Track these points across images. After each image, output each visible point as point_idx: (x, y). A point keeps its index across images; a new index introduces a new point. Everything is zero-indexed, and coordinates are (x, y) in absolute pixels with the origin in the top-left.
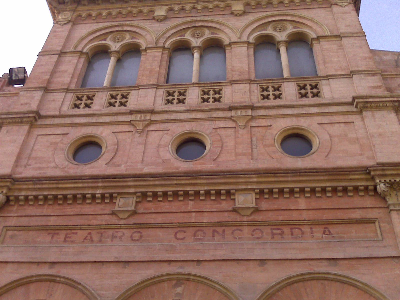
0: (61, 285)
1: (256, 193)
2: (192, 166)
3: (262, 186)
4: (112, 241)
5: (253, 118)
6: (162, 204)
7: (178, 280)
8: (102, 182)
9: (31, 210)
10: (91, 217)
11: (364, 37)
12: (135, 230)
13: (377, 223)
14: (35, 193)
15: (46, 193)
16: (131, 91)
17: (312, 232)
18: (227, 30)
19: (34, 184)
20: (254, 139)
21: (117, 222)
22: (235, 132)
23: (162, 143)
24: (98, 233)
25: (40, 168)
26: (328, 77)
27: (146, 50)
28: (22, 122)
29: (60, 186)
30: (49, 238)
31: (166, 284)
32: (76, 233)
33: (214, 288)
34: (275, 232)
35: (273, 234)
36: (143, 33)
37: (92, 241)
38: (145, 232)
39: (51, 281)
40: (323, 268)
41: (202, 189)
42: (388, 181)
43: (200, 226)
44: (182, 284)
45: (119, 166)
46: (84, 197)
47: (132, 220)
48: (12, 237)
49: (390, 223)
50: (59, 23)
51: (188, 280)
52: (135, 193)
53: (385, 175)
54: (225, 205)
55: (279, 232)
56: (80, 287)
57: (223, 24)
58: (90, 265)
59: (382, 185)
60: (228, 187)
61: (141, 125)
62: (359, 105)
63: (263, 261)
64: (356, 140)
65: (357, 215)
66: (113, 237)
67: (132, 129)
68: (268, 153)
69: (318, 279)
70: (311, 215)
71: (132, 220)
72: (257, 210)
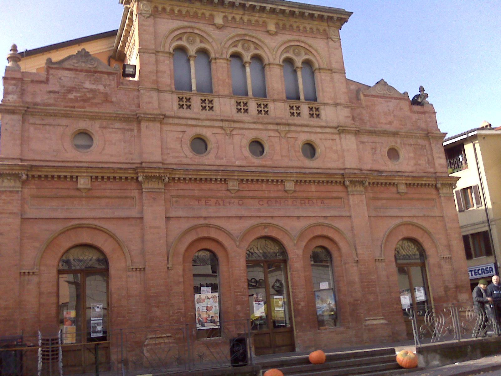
0: (212, 228)
1: (294, 182)
2: (261, 162)
3: (297, 179)
4: (230, 205)
5: (289, 131)
6: (250, 185)
7: (265, 226)
8: (221, 173)
9: (182, 186)
10: (216, 191)
11: (344, 74)
12: (239, 199)
13: (342, 199)
14: (184, 177)
15: (190, 177)
16: (214, 98)
17: (317, 203)
18: (265, 49)
19: (184, 172)
20: (290, 146)
21: (230, 195)
22: (279, 140)
23: (243, 144)
24: (221, 200)
25: (177, 157)
26: (325, 104)
27: (215, 59)
28: (155, 121)
29: (199, 173)
30: (197, 203)
31: (260, 228)
32: (210, 200)
33: (280, 229)
34: (302, 202)
35: (301, 203)
36: (210, 40)
37: (219, 205)
38: (246, 201)
39: (207, 227)
40: (321, 221)
41: (270, 179)
42: (350, 180)
43: (269, 199)
44: (267, 227)
45: (222, 159)
46: (211, 179)
47: (238, 194)
48: (176, 202)
49: (348, 200)
50: (143, 15)
51: (269, 226)
52: (238, 179)
53: (350, 177)
54: (280, 187)
55: (304, 202)
56: (223, 229)
57: (263, 42)
58: (224, 218)
59: (348, 182)
60: (282, 179)
61: (229, 130)
62: (340, 131)
63: (298, 217)
64: (336, 152)
65: (335, 195)
66: (230, 203)
67: (223, 132)
68: (297, 157)
69: (320, 225)
70: (317, 194)
71: (238, 194)
72: (295, 191)
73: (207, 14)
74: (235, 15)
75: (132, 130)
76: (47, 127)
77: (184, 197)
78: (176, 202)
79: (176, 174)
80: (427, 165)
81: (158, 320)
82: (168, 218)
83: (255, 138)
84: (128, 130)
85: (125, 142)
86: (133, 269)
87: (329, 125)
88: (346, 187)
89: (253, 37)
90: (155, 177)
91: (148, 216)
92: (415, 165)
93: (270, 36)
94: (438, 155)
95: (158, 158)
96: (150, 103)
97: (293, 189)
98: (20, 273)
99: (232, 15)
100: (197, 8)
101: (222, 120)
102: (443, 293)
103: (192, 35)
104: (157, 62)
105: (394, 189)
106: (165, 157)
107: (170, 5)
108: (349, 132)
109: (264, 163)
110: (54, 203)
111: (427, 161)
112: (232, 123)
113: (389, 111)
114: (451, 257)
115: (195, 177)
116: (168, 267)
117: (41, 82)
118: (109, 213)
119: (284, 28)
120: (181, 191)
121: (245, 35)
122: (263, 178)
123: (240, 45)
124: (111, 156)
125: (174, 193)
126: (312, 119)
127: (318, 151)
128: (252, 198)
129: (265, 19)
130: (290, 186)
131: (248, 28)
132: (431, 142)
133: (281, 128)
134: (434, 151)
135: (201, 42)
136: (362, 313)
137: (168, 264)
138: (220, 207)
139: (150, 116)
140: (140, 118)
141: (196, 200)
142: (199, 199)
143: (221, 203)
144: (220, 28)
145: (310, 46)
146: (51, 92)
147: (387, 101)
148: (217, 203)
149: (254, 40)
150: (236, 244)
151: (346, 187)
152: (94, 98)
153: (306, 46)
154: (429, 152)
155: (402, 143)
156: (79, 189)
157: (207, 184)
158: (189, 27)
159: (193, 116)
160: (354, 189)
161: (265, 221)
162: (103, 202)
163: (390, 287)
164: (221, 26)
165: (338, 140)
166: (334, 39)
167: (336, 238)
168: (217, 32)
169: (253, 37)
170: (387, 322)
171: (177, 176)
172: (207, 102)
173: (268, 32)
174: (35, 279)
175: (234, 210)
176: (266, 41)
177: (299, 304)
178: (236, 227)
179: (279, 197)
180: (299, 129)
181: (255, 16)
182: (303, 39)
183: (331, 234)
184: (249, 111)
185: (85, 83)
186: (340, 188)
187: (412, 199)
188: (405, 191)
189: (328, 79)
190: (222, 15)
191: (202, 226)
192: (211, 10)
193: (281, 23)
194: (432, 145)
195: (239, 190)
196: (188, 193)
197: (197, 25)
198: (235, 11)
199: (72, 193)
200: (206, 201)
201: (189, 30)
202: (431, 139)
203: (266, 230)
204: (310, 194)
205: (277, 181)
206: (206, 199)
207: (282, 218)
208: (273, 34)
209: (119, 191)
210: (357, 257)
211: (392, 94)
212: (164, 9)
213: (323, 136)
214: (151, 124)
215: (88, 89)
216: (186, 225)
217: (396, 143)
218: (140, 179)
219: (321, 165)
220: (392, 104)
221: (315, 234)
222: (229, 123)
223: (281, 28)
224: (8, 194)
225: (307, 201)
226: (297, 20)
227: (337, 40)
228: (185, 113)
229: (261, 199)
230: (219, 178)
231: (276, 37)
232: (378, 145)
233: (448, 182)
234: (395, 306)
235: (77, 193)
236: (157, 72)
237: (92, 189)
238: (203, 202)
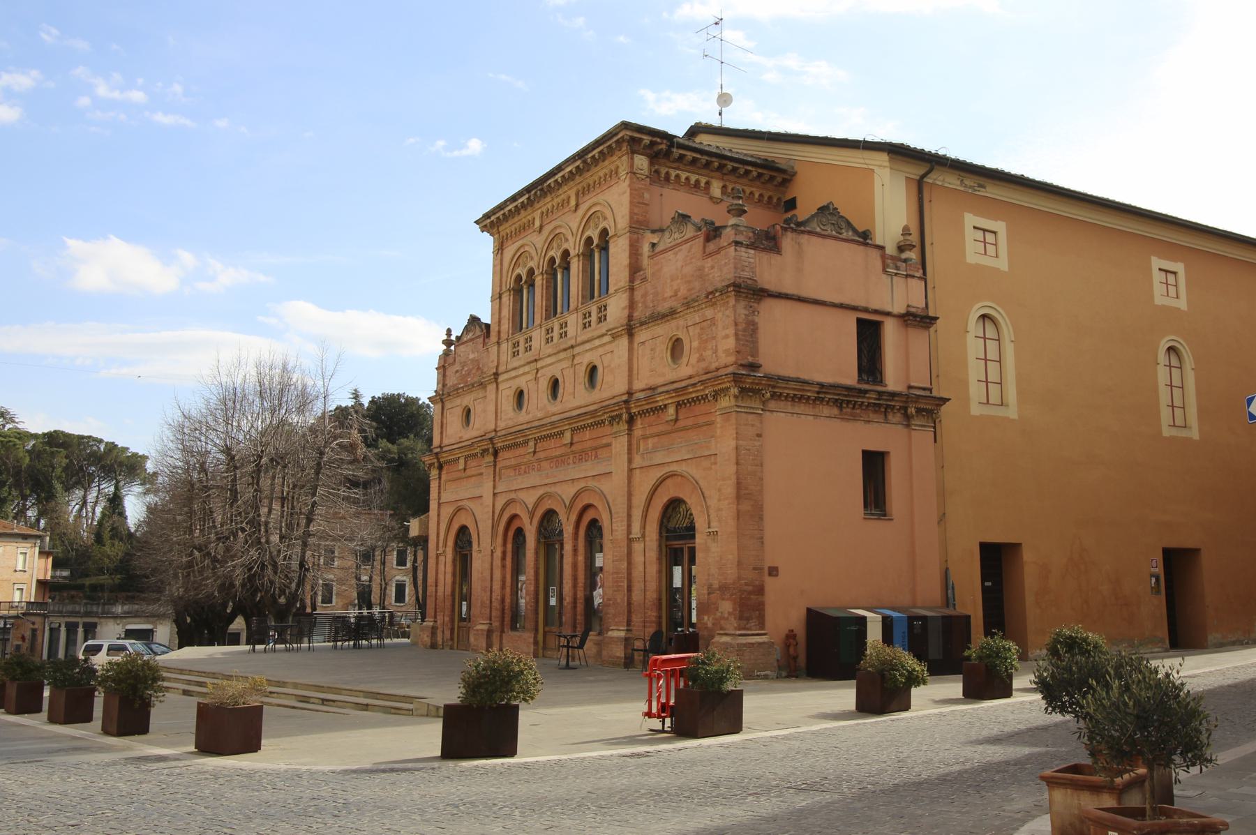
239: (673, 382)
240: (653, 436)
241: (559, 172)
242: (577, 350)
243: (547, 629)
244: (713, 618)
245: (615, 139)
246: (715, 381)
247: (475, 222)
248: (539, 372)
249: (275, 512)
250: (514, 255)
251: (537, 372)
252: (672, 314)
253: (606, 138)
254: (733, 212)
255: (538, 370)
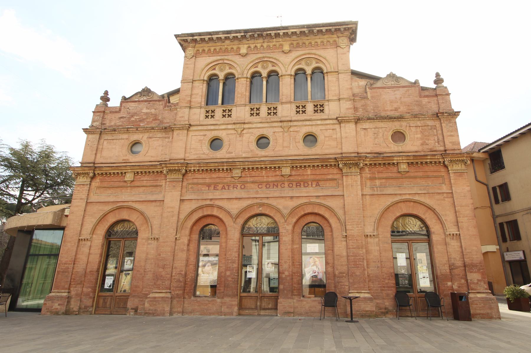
18: (280, 65)
21: (234, 181)
27: (238, 79)
30: (207, 188)
32: (218, 186)
36: (235, 66)
40: (313, 200)
43: (268, 183)
45: (232, 153)
48: (192, 188)
57: (278, 60)
60: (279, 165)
63: (292, 197)
65: (330, 177)
70: (312, 177)
72: (290, 175)
73: (235, 47)
74: (256, 44)
75: (169, 138)
76: (115, 141)
77: (198, 184)
78: (192, 188)
79: (191, 167)
80: (437, 144)
81: (162, 278)
82: (182, 201)
83: (305, 134)
84: (166, 138)
85: (162, 146)
86: (151, 238)
87: (330, 117)
88: (341, 170)
89: (270, 58)
90: (175, 170)
91: (168, 200)
92: (422, 144)
93: (285, 54)
94: (449, 134)
95: (182, 156)
96: (182, 117)
97: (289, 174)
98: (79, 239)
99: (254, 45)
100: (227, 45)
101: (234, 124)
102: (448, 271)
103: (222, 64)
104: (192, 88)
105: (395, 169)
106: (187, 155)
107: (208, 47)
108: (348, 121)
109: (267, 154)
110: (109, 191)
111: (436, 140)
112: (290, 122)
113: (396, 98)
114: (459, 234)
115: (206, 168)
116: (176, 238)
117: (116, 112)
118: (143, 198)
119: (298, 46)
120: (196, 180)
121: (264, 57)
122: (262, 166)
123: (260, 66)
124: (152, 157)
125: (191, 181)
126: (316, 114)
127: (319, 140)
128: (253, 182)
129: (281, 42)
130: (286, 171)
131: (268, 52)
132: (442, 122)
133: (285, 124)
134: (445, 130)
135: (230, 68)
136: (346, 286)
137: (176, 235)
138: (225, 191)
139: (179, 126)
140: (172, 129)
141: (207, 186)
142: (209, 185)
143: (227, 188)
144: (244, 56)
145: (320, 56)
146: (121, 118)
147: (395, 91)
148: (224, 188)
149: (271, 60)
150: (233, 220)
151: (446, 166)
152: (147, 118)
153: (316, 57)
154: (440, 132)
155: (408, 125)
156: (125, 182)
157: (208, 174)
158: (220, 60)
159: (308, 118)
160: (348, 171)
161: (261, 202)
162: (141, 189)
163: (381, 262)
164: (245, 54)
165: (338, 130)
166: (342, 47)
167: (327, 215)
168: (242, 59)
169: (270, 58)
170: (372, 297)
171: (193, 168)
172: (319, 106)
173: (283, 51)
174: (89, 243)
175: (235, 193)
176: (280, 59)
177: (284, 273)
178: (235, 207)
179: (276, 181)
180: (300, 123)
181: (273, 42)
182: (314, 51)
183: (322, 211)
184: (260, 114)
185: (143, 109)
186: (335, 171)
187: (415, 178)
188: (407, 170)
189: (335, 79)
190: (246, 46)
191: (207, 206)
192: (238, 45)
193: (295, 43)
194: (443, 125)
195: (241, 177)
196: (201, 181)
197: (226, 57)
198: (256, 41)
199: (122, 184)
200: (214, 186)
201: (220, 62)
202: (442, 119)
203: (261, 209)
204: (306, 177)
205: (275, 167)
206: (215, 185)
207: (277, 198)
208: (287, 53)
209: (152, 181)
210: (346, 233)
211: (403, 84)
212: (204, 50)
213: (323, 127)
214: (180, 132)
215: (144, 113)
216: (194, 205)
217: (401, 126)
218: (341, 166)
219: (271, 153)
220: (399, 93)
221: (306, 212)
222: (240, 125)
223: (295, 47)
224: (82, 186)
225: (302, 184)
226: (309, 38)
227: (345, 47)
228: (210, 121)
229: (261, 183)
230: (225, 168)
231: (290, 54)
232: (380, 130)
233: (458, 159)
234: (387, 281)
235: (125, 184)
236: (191, 95)
237: (408, 172)
238: (212, 187)
239: (401, 152)
240: (380, 179)
241: (282, 30)
242: (246, 126)
243: (100, 294)
244: (458, 284)
245: (344, 27)
246: (456, 155)
247: (175, 35)
248: (245, 130)
249: (4, 184)
250: (211, 63)
251: (243, 130)
252: (400, 118)
253: (270, 29)
254: (103, 99)
255: (244, 129)
